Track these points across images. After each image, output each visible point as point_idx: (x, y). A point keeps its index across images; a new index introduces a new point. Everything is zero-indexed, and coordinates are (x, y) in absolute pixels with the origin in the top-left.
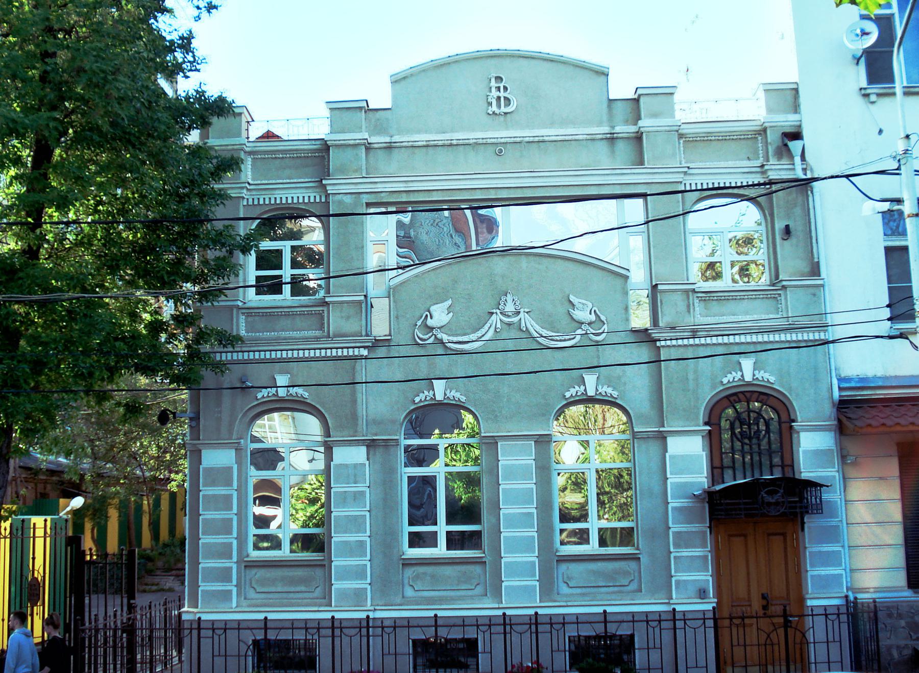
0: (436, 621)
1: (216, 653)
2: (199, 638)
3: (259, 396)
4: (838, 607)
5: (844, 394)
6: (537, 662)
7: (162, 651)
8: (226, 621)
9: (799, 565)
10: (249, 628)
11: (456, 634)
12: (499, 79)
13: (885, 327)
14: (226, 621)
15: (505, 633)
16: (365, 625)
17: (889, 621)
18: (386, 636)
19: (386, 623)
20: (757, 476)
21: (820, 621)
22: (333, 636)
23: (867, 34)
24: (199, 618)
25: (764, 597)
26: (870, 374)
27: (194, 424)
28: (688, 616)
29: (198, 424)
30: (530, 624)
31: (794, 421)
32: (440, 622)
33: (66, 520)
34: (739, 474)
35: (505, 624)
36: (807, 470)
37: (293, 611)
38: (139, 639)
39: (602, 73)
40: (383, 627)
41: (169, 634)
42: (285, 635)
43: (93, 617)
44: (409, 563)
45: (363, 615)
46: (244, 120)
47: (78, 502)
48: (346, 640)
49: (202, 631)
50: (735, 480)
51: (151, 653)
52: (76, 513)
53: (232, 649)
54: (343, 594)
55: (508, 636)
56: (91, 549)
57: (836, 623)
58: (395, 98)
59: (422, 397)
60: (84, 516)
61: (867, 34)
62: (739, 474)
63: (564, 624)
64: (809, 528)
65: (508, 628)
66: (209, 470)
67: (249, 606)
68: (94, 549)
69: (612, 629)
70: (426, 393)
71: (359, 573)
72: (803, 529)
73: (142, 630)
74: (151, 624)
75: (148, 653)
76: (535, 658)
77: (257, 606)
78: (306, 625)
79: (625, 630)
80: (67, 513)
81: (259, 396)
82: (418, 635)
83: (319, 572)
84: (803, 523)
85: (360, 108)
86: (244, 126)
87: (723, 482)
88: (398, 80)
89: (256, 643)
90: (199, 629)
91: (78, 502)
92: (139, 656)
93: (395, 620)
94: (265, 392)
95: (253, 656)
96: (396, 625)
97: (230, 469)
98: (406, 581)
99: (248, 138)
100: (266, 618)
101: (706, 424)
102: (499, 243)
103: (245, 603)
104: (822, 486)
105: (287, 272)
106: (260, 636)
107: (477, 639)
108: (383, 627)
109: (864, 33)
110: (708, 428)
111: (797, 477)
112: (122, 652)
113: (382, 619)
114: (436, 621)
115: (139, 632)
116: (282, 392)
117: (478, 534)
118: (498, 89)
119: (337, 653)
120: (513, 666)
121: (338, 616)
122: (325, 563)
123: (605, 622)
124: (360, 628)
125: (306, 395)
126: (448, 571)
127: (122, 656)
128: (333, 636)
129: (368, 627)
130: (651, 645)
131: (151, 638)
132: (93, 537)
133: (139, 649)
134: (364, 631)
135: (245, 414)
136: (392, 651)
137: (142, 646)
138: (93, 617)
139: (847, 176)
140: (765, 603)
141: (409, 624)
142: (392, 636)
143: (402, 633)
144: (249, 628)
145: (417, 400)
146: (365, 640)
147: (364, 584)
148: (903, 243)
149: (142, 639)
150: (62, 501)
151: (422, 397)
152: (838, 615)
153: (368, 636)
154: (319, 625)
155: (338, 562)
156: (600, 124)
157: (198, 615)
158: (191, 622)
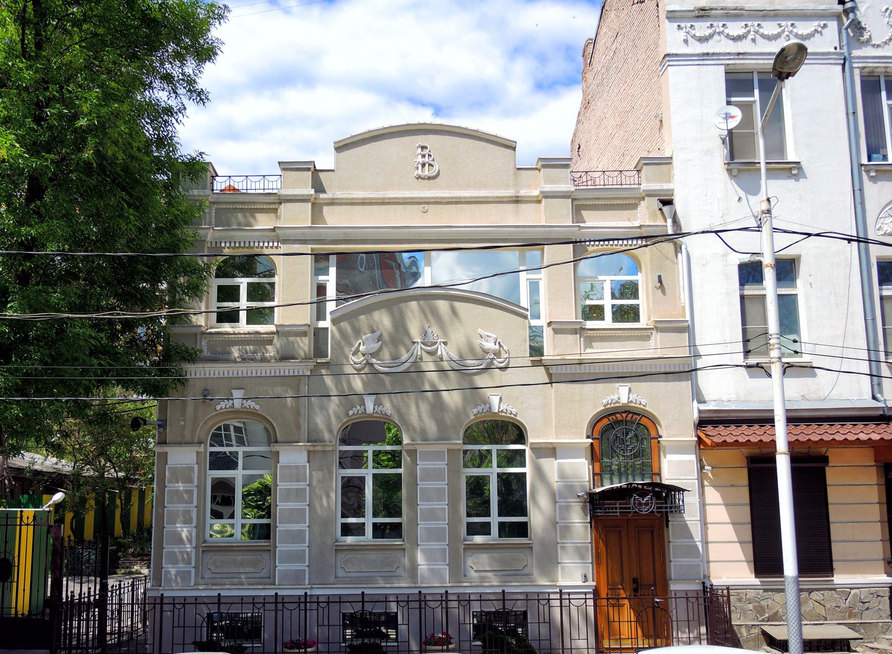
0: (219, 600)
1: (176, 624)
2: (162, 611)
3: (218, 407)
4: (697, 591)
5: (703, 415)
6: (447, 633)
7: (129, 623)
8: (185, 598)
9: (664, 556)
10: (204, 603)
11: (379, 609)
12: (423, 148)
13: (740, 359)
14: (686, 591)
15: (420, 608)
16: (304, 601)
17: (738, 604)
18: (320, 610)
19: (321, 599)
20: (631, 481)
21: (682, 603)
22: (276, 610)
23: (732, 117)
24: (162, 595)
25: (635, 581)
26: (725, 398)
27: (162, 430)
28: (428, 598)
29: (165, 430)
30: (155, 604)
31: (661, 437)
32: (222, 601)
33: (49, 512)
34: (616, 479)
35: (276, 603)
36: (668, 477)
37: (240, 587)
38: (109, 613)
39: (511, 146)
40: (318, 603)
41: (136, 607)
42: (234, 610)
43: (69, 594)
44: (339, 549)
45: (302, 593)
46: (209, 174)
47: (58, 497)
48: (287, 613)
49: (365, 604)
50: (612, 484)
51: (120, 625)
52: (58, 506)
53: (190, 622)
54: (285, 575)
55: (423, 610)
56: (69, 537)
57: (696, 605)
58: (337, 162)
59: (355, 410)
60: (64, 508)
61: (732, 117)
62: (616, 479)
63: (184, 604)
64: (673, 525)
65: (423, 603)
66: (174, 471)
67: (249, 584)
68: (72, 538)
69: (368, 607)
70: (358, 407)
71: (298, 557)
72: (667, 526)
73: (112, 604)
74: (120, 600)
75: (117, 625)
76: (445, 630)
77: (252, 584)
78: (253, 601)
79: (520, 607)
80: (49, 506)
81: (218, 407)
82: (348, 609)
83: (266, 556)
84: (668, 521)
85: (309, 169)
86: (209, 179)
87: (602, 486)
88: (341, 147)
89: (210, 616)
90: (162, 604)
91: (58, 497)
92: (109, 629)
93: (329, 596)
94: (223, 405)
95: (208, 627)
96: (329, 601)
97: (192, 469)
98: (338, 565)
99: (213, 190)
100: (219, 595)
101: (588, 437)
102: (867, 184)
103: (202, 581)
104: (684, 490)
105: (244, 303)
106: (214, 609)
107: (397, 613)
108: (318, 603)
109: (728, 117)
110: (590, 441)
111: (663, 482)
112: (94, 624)
113: (318, 596)
114: (219, 600)
115: (109, 607)
116: (237, 404)
117: (398, 526)
118: (424, 156)
119: (423, 626)
120: (426, 637)
121: (280, 593)
122: (271, 548)
123: (363, 602)
124: (300, 603)
125: (257, 407)
126: (373, 556)
127: (94, 627)
128: (276, 610)
129: (306, 602)
130: (541, 620)
131: (119, 612)
132: (71, 528)
133: (109, 622)
134: (302, 605)
135: (205, 423)
136: (181, 624)
137: (112, 619)
138: (69, 594)
139: (716, 232)
140: (635, 586)
141: (341, 600)
142: (326, 610)
143: (335, 608)
144: (204, 603)
145: (351, 413)
146: (303, 612)
147: (303, 566)
148: (761, 292)
149: (112, 614)
150: (45, 497)
151: (355, 410)
152: (697, 598)
153: (306, 610)
154: (264, 601)
155: (281, 547)
156: (507, 187)
157: (161, 592)
158: (155, 598)
